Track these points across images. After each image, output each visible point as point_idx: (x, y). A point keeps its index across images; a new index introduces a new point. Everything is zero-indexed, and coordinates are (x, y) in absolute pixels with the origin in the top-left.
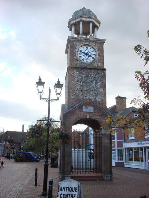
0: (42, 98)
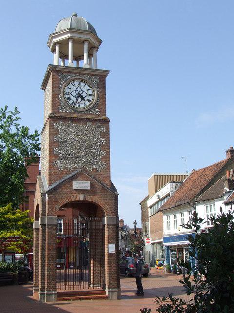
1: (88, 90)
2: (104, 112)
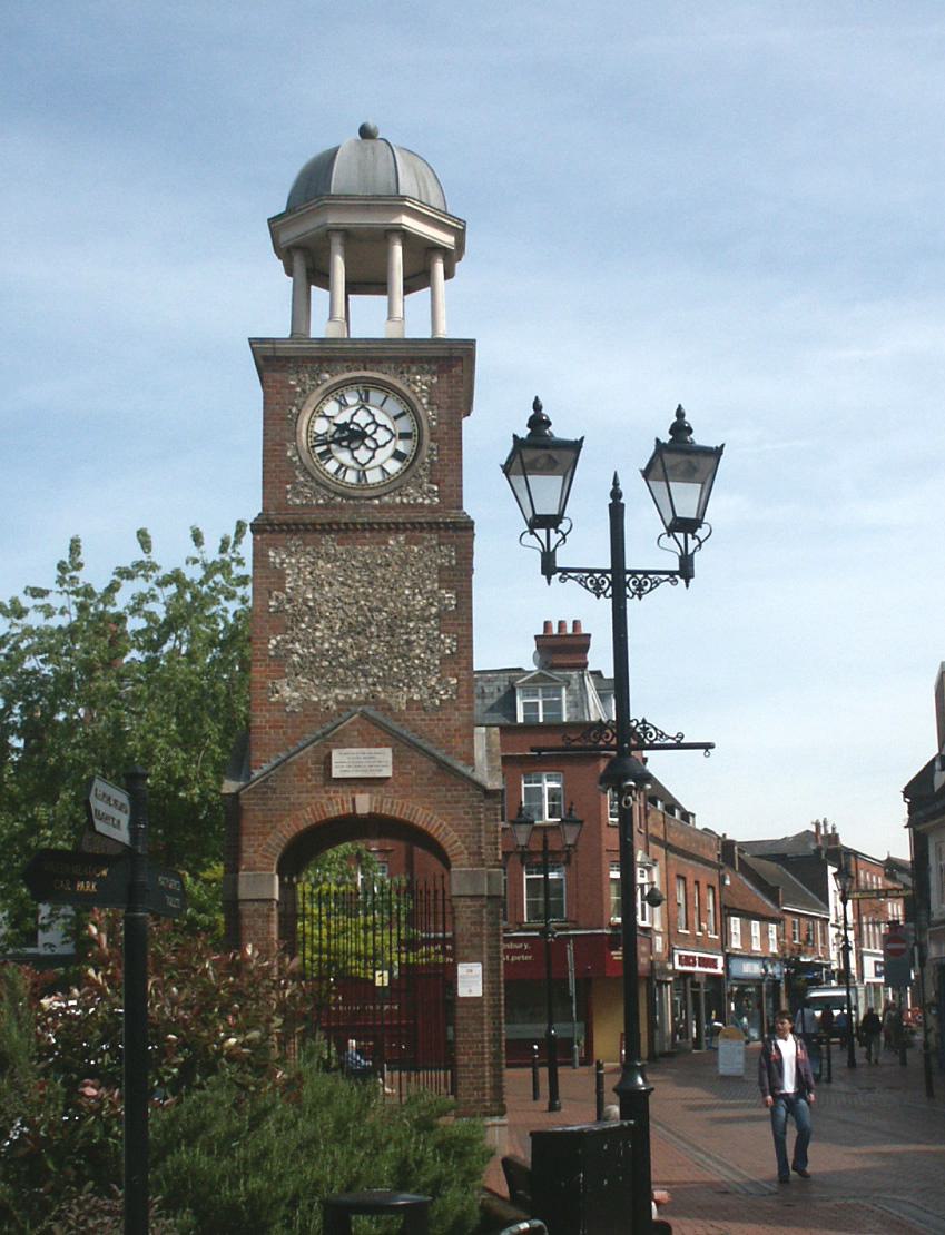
0: (561, 561)
1: (396, 418)
2: (454, 496)
